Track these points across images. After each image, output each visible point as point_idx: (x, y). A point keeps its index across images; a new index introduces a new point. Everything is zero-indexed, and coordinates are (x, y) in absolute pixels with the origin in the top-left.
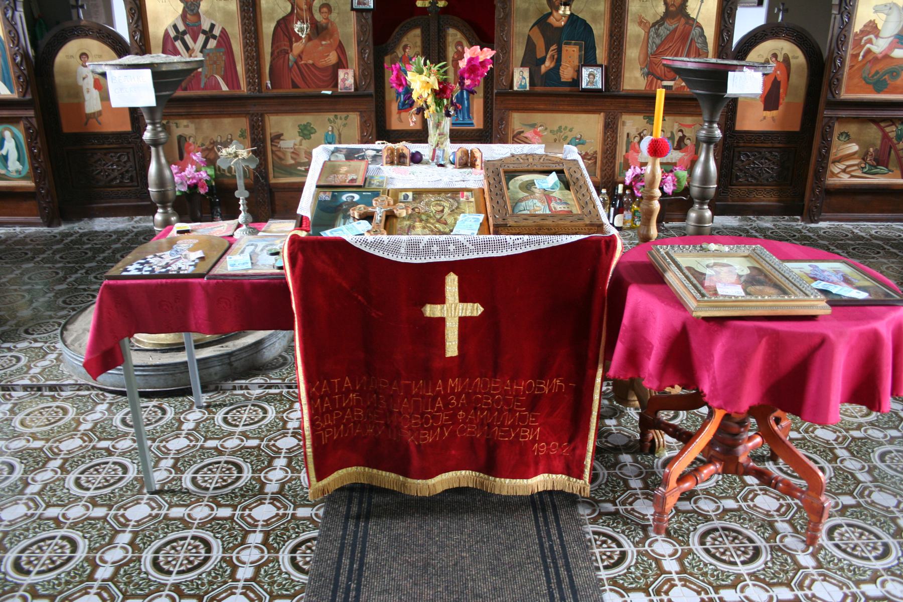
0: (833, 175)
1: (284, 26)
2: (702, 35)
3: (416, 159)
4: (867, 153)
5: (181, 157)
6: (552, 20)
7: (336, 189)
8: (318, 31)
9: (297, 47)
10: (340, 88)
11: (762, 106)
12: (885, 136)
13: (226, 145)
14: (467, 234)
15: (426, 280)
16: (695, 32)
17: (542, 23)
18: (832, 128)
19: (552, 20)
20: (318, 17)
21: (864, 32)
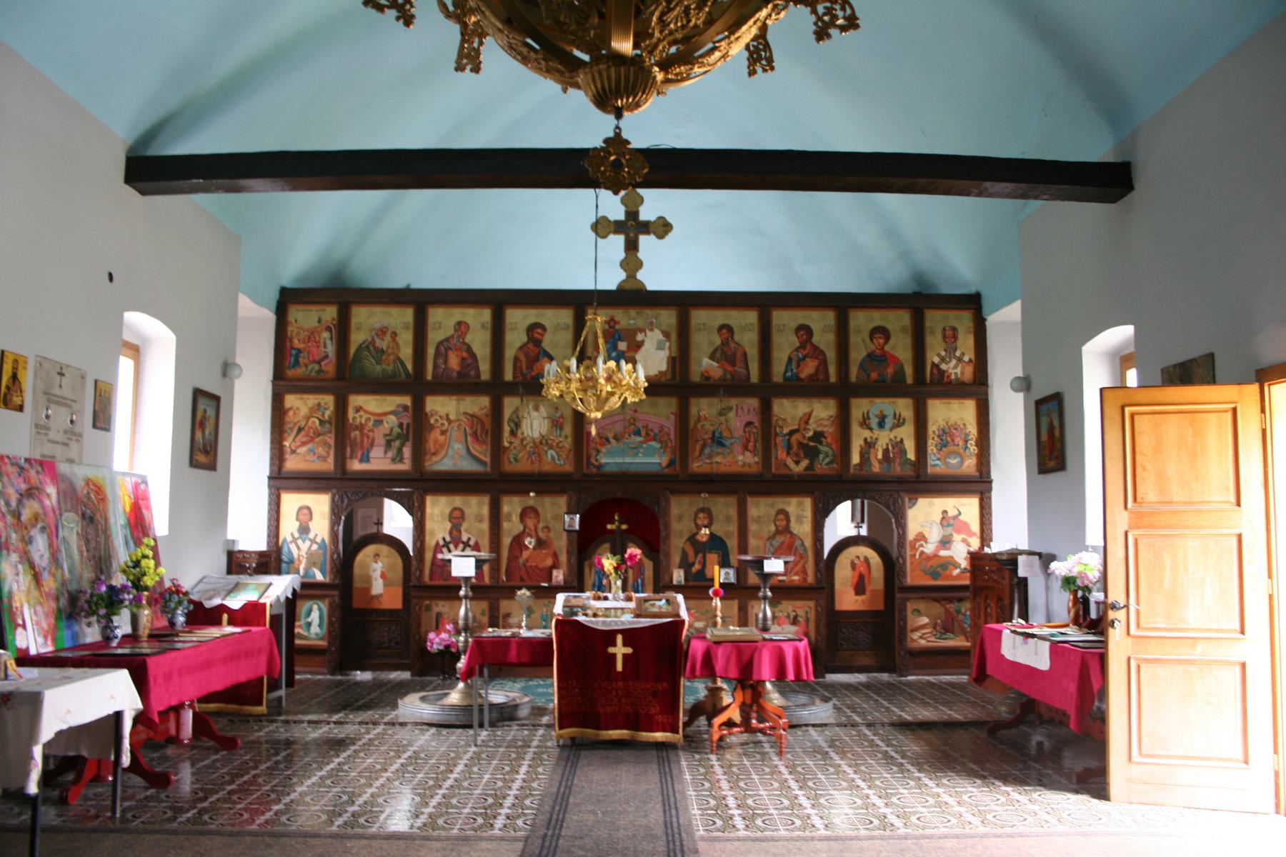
0: (913, 640)
1: (518, 541)
2: (803, 545)
3: (606, 598)
4: (936, 624)
5: (437, 628)
6: (698, 537)
7: (571, 607)
8: (541, 543)
9: (526, 554)
10: (554, 582)
11: (852, 592)
12: (947, 611)
13: (520, 588)
14: (627, 620)
15: (609, 637)
16: (798, 543)
17: (692, 539)
18: (905, 605)
19: (698, 537)
20: (541, 535)
21: (916, 540)
